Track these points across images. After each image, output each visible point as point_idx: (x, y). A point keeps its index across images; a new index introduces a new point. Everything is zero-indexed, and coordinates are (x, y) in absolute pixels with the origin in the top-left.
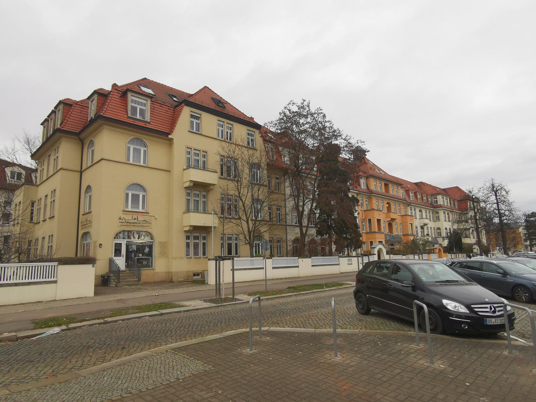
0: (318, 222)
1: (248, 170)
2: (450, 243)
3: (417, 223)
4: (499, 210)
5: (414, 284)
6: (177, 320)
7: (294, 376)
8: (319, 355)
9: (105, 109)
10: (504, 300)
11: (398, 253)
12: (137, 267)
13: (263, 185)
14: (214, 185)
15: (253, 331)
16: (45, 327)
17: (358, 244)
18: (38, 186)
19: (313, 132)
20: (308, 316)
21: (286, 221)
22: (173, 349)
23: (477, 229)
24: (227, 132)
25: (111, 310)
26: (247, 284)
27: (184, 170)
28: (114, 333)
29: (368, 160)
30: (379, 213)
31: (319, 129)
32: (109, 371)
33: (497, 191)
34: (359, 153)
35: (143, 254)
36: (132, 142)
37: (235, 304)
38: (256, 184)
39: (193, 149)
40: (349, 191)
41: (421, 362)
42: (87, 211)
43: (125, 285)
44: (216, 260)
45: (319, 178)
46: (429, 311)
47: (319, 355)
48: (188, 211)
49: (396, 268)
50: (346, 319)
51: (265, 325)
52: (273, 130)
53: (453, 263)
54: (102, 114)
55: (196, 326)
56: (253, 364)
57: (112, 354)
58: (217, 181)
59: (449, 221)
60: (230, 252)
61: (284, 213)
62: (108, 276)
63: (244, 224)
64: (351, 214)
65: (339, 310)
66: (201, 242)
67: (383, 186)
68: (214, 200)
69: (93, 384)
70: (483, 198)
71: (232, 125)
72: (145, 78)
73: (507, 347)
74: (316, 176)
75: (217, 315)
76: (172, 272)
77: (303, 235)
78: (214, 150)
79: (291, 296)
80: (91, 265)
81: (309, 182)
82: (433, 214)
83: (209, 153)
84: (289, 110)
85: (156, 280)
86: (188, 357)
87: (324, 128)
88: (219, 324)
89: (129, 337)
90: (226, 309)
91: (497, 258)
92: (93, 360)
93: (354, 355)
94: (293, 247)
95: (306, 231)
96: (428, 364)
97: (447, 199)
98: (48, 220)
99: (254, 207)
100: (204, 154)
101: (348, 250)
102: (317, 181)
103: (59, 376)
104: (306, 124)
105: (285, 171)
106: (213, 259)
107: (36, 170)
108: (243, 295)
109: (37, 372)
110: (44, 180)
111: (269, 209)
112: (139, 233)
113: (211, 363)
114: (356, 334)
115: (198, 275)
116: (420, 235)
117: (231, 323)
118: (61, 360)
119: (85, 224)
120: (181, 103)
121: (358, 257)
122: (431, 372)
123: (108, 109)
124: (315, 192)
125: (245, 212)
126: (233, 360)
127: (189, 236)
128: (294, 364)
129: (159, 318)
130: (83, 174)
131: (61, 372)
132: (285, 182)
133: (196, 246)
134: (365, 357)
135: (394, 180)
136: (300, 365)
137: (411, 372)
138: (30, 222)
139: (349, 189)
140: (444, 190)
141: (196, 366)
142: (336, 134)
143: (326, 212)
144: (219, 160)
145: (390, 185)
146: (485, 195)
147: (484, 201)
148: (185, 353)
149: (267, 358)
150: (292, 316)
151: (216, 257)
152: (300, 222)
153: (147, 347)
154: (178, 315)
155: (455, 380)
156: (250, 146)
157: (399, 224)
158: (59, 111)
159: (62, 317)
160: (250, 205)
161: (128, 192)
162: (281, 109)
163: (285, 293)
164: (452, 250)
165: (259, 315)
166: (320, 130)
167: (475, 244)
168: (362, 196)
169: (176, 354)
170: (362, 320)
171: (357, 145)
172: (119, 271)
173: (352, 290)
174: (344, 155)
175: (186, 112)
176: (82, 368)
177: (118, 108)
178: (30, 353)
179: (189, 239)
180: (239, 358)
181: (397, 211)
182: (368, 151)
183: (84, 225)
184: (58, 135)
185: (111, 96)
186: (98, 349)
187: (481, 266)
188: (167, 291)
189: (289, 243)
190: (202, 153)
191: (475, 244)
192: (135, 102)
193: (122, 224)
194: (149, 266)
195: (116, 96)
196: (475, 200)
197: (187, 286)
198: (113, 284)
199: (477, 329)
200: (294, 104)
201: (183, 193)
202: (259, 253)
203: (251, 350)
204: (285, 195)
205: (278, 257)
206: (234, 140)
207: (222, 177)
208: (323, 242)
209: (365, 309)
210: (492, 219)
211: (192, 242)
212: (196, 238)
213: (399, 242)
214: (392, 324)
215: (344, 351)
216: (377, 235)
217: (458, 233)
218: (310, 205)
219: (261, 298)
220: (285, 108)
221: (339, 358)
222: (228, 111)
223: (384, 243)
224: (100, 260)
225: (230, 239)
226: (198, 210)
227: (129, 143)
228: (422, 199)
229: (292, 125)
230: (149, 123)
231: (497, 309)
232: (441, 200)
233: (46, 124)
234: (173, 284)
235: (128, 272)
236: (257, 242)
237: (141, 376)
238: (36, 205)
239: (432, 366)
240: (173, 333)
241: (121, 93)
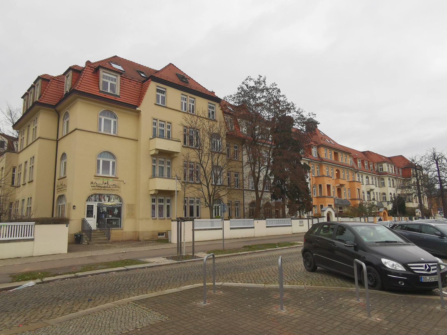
0: (273, 187)
1: (208, 140)
2: (394, 207)
3: (364, 188)
4: (439, 177)
5: (356, 244)
6: (141, 275)
7: (242, 327)
8: (266, 308)
9: (79, 84)
10: (438, 259)
11: (345, 215)
12: (108, 227)
13: (221, 153)
14: (178, 153)
15: (207, 286)
16: (22, 280)
17: (309, 208)
18: (19, 153)
19: (268, 105)
20: (259, 273)
21: (243, 186)
22: (134, 301)
23: (419, 194)
24: (190, 105)
25: (82, 266)
26: (207, 243)
27: (151, 139)
28: (83, 286)
29: (319, 131)
30: (329, 179)
31: (275, 103)
32: (75, 321)
33: (438, 159)
34: (311, 125)
35: (113, 215)
36: (103, 113)
37: (195, 261)
38: (216, 152)
39: (158, 120)
40: (302, 159)
41: (360, 315)
42: (62, 176)
43: (96, 243)
44: (178, 221)
45: (274, 147)
46: (367, 269)
47: (266, 308)
48: (154, 176)
49: (342, 229)
50: (294, 275)
51: (219, 280)
52: (232, 103)
53: (395, 225)
54: (76, 88)
55: (157, 280)
56: (206, 315)
57: (79, 305)
58: (180, 149)
59: (394, 187)
60: (192, 214)
61: (241, 179)
62: (81, 235)
63: (205, 189)
64: (303, 180)
65: (289, 267)
66: (165, 205)
67: (333, 155)
68: (177, 166)
69: (60, 332)
70: (426, 166)
71: (195, 98)
72: (116, 56)
73: (440, 302)
74: (271, 145)
75: (177, 270)
76: (139, 232)
77: (259, 199)
78: (178, 122)
79: (246, 254)
80: (65, 225)
81: (265, 151)
82: (378, 180)
83: (173, 124)
84: (247, 86)
85: (125, 239)
86: (147, 309)
87: (279, 102)
88: (178, 280)
89: (96, 290)
90: (186, 265)
91: (437, 222)
92: (62, 311)
93: (298, 308)
94: (250, 209)
95: (262, 195)
96: (366, 318)
97: (392, 167)
98: (27, 183)
99: (214, 173)
100: (169, 124)
101: (300, 212)
102: (272, 150)
103: (30, 324)
104: (262, 97)
105: (242, 141)
106: (175, 220)
107: (17, 139)
108: (202, 253)
109: (11, 321)
110: (24, 147)
111: (228, 175)
112: (109, 196)
113: (167, 315)
114: (302, 290)
115: (163, 234)
116: (366, 199)
117: (189, 278)
118: (33, 310)
119: (60, 187)
120: (148, 79)
121: (308, 219)
122: (368, 325)
123: (82, 83)
124: (270, 159)
125: (206, 178)
126: (188, 312)
127: (154, 199)
128: (243, 316)
129: (125, 273)
130: (59, 143)
131: (32, 321)
132: (242, 151)
133: (161, 208)
134: (308, 310)
135: (343, 149)
136: (248, 317)
137: (350, 324)
138: (11, 186)
139: (301, 158)
140: (390, 158)
141: (154, 317)
142: (289, 107)
143: (280, 177)
144: (182, 130)
145: (339, 154)
146: (427, 163)
147: (426, 169)
148: (145, 305)
149: (219, 310)
150: (246, 272)
151: (177, 218)
152: (256, 188)
153: (112, 299)
154: (142, 271)
155: (390, 332)
156: (211, 117)
157: (347, 189)
158: (37, 85)
159: (38, 271)
160: (210, 171)
161: (99, 159)
162: (239, 84)
163: (241, 252)
164: (396, 213)
165: (215, 272)
166: (275, 103)
167: (417, 208)
168: (313, 163)
169: (137, 306)
170: (309, 276)
171: (308, 117)
172: (90, 230)
173: (300, 250)
174: (297, 126)
175: (153, 86)
176: (51, 317)
177: (91, 83)
178: (6, 303)
179: (154, 202)
180: (193, 310)
181: (346, 177)
182: (318, 124)
183: (59, 189)
184: (37, 107)
185: (84, 72)
186: (67, 301)
187: (420, 228)
188: (133, 249)
189: (246, 206)
190: (167, 124)
191: (417, 208)
192: (107, 78)
193: (94, 188)
194: (118, 226)
195: (89, 72)
196: (418, 168)
197: (152, 244)
198: (85, 242)
199: (412, 285)
200: (251, 79)
201: (150, 160)
202: (218, 215)
203: (205, 303)
204: (242, 162)
205: (236, 218)
206: (196, 112)
207: (185, 146)
208: (277, 205)
209: (312, 267)
210: (434, 185)
211: (157, 204)
212: (161, 201)
213: (348, 206)
214: (336, 280)
215: (290, 305)
216: (327, 199)
217: (402, 198)
218: (265, 172)
219: (215, 256)
220: (243, 83)
221: (284, 312)
222: (191, 86)
223: (333, 206)
224: (73, 220)
225: (192, 202)
226: (163, 175)
227: (101, 114)
228: (369, 167)
229: (250, 99)
230: (119, 96)
231: (432, 268)
232: (386, 167)
233: (26, 97)
234: (140, 242)
235: (99, 231)
236: (217, 205)
237: (103, 325)
238: (17, 170)
239: (370, 319)
240: (136, 287)
241: (93, 69)
